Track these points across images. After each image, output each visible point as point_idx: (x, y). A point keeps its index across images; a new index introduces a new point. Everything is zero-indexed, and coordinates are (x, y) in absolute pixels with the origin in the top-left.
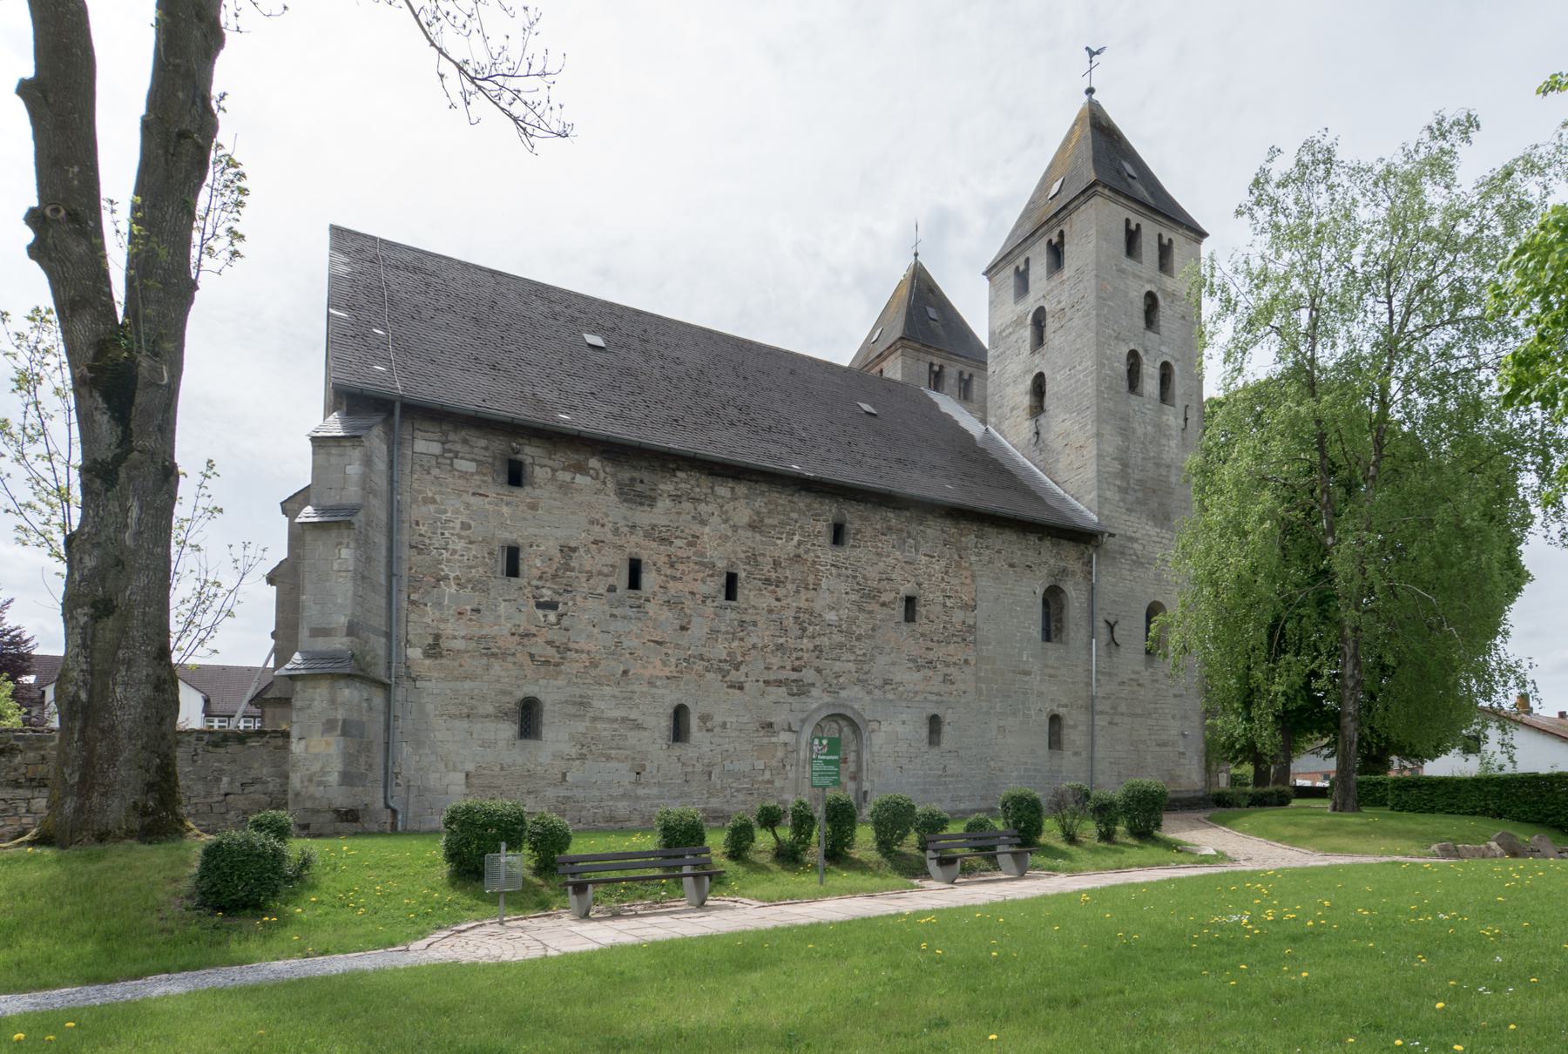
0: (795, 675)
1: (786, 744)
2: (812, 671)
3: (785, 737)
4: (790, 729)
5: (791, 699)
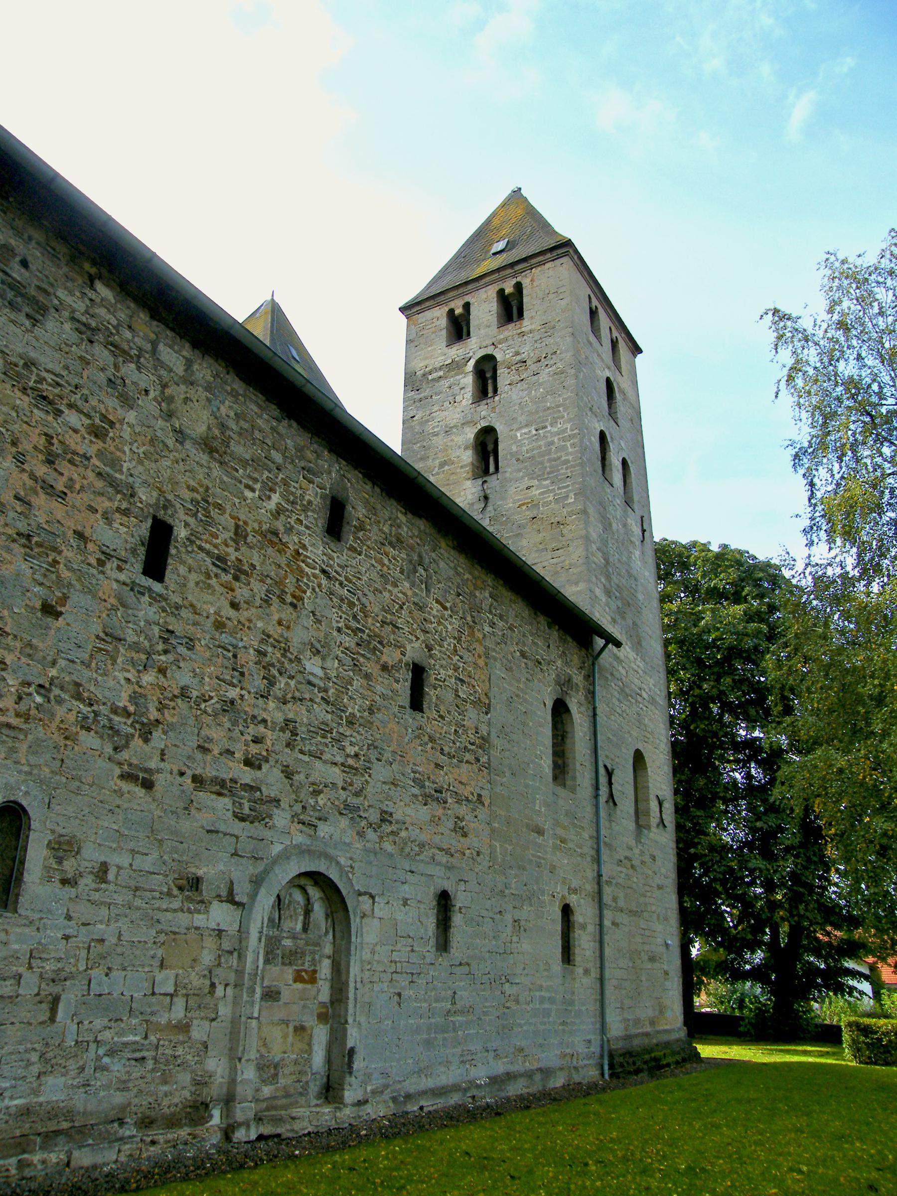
0: (247, 776)
1: (220, 932)
2: (277, 773)
3: (220, 915)
4: (231, 899)
5: (238, 827)
